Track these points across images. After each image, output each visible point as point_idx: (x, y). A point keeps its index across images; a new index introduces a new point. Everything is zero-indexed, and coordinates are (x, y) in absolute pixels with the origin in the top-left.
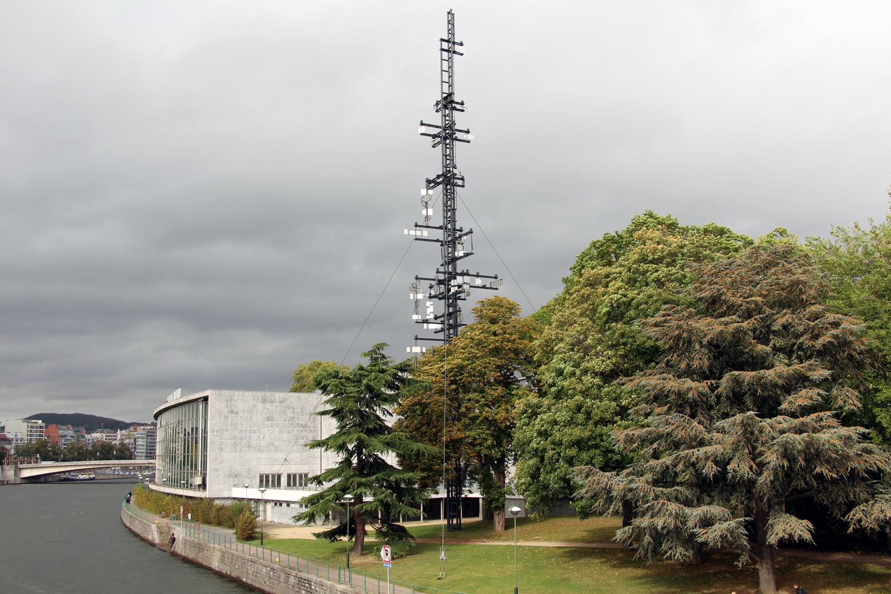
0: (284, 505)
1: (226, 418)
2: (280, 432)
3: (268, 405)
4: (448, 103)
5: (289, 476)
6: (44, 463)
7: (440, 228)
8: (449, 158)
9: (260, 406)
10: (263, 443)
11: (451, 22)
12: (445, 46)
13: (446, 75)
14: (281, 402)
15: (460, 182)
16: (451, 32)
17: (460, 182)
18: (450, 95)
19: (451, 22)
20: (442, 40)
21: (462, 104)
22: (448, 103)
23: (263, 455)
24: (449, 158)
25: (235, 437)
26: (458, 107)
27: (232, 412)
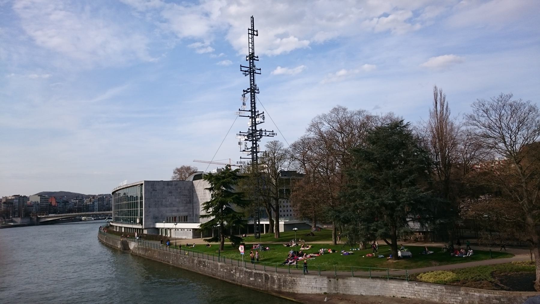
0: (180, 230)
1: (151, 193)
2: (175, 198)
3: (170, 187)
4: (252, 57)
5: (179, 217)
6: (50, 215)
7: (250, 111)
8: (252, 81)
9: (166, 187)
10: (168, 203)
11: (253, 21)
12: (250, 32)
13: (251, 45)
14: (175, 185)
15: (257, 91)
16: (253, 26)
17: (257, 91)
18: (253, 53)
19: (253, 21)
20: (249, 29)
21: (257, 57)
22: (252, 57)
23: (168, 209)
24: (252, 81)
25: (156, 201)
26: (256, 59)
27: (154, 190)
